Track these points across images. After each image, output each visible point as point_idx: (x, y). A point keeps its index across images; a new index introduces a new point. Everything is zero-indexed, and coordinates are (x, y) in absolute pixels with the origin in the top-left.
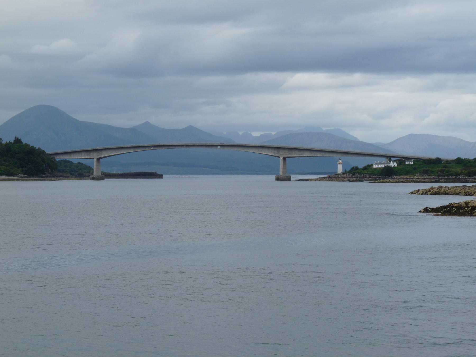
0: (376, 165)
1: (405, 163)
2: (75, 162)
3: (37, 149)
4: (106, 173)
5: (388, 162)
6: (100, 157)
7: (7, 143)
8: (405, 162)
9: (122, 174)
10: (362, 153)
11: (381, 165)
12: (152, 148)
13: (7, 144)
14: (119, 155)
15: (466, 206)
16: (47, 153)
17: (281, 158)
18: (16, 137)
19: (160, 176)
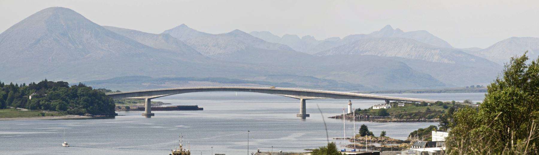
0: (375, 107)
9: (166, 107)
11: (379, 107)
17: (301, 100)
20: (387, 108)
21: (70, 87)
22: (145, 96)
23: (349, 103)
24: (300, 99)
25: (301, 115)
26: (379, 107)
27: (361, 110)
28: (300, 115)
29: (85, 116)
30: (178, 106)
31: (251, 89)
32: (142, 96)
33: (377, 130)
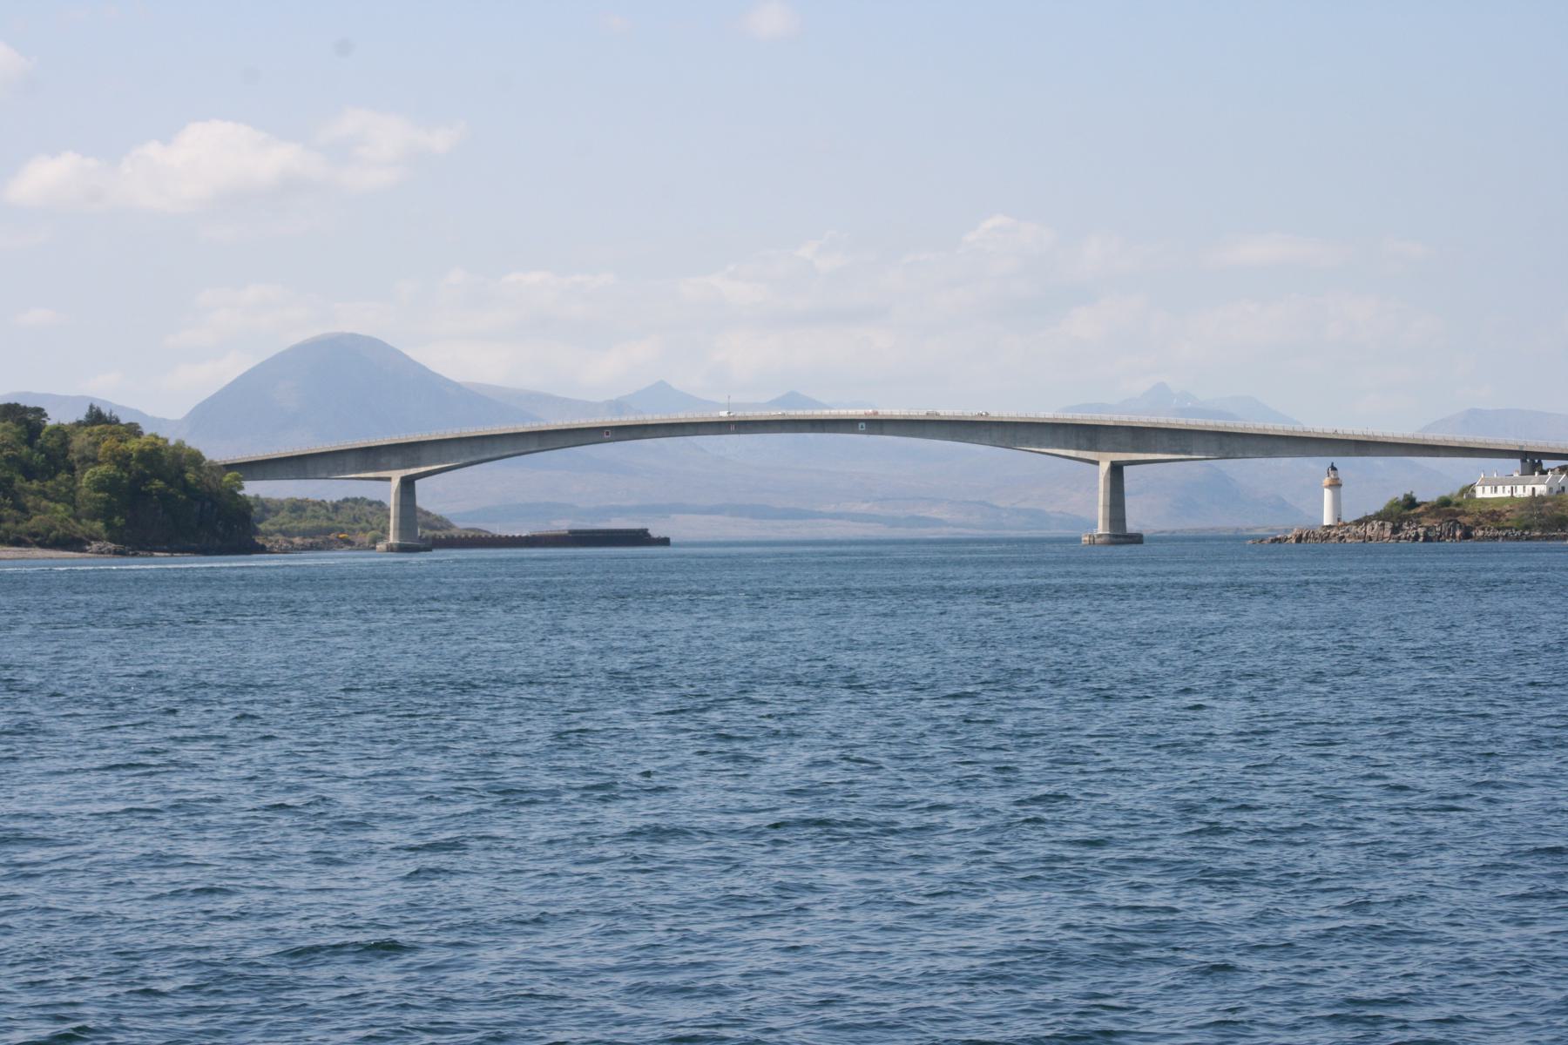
0: (1488, 488)
4: (483, 535)
5: (1516, 475)
9: (527, 537)
10: (1424, 440)
14: (449, 473)
15: (100, 495)
17: (1105, 466)
18: (91, 407)
20: (1550, 490)
23: (1327, 481)
24: (1097, 463)
25: (1102, 539)
26: (1508, 488)
27: (1418, 505)
28: (1100, 536)
29: (86, 551)
30: (570, 532)
33: (998, 532)
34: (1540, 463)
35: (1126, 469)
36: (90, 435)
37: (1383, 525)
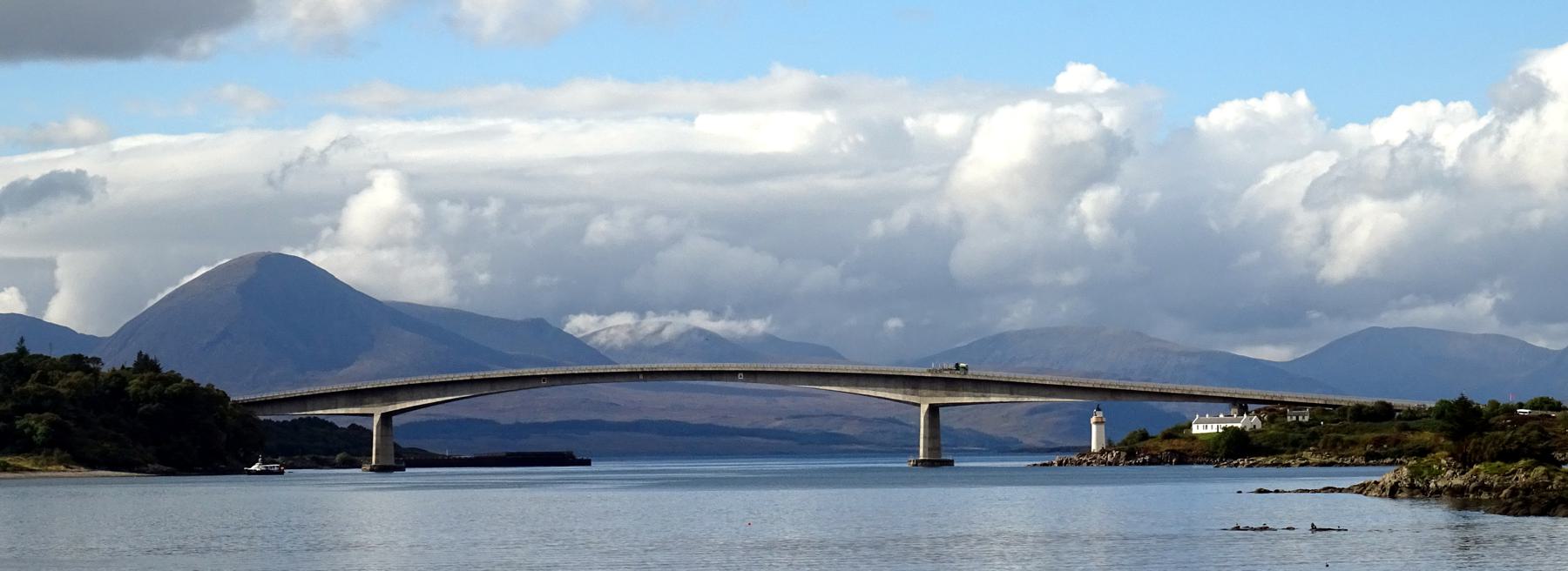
0: (1201, 426)
1: (1309, 96)
2: (343, 424)
3: (202, 388)
5: (1235, 416)
6: (391, 408)
7: (114, 370)
8: (1285, 414)
11: (1215, 426)
12: (544, 381)
13: (114, 374)
16: (1504, 405)
17: (924, 408)
18: (140, 354)
19: (587, 463)
21: (1308, 312)
22: (370, 403)
31: (744, 372)
32: (361, 404)
34: (1246, 408)
35: (941, 410)
36: (141, 379)
37: (1119, 453)
